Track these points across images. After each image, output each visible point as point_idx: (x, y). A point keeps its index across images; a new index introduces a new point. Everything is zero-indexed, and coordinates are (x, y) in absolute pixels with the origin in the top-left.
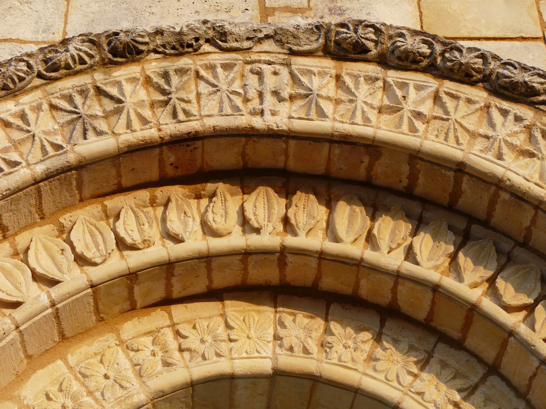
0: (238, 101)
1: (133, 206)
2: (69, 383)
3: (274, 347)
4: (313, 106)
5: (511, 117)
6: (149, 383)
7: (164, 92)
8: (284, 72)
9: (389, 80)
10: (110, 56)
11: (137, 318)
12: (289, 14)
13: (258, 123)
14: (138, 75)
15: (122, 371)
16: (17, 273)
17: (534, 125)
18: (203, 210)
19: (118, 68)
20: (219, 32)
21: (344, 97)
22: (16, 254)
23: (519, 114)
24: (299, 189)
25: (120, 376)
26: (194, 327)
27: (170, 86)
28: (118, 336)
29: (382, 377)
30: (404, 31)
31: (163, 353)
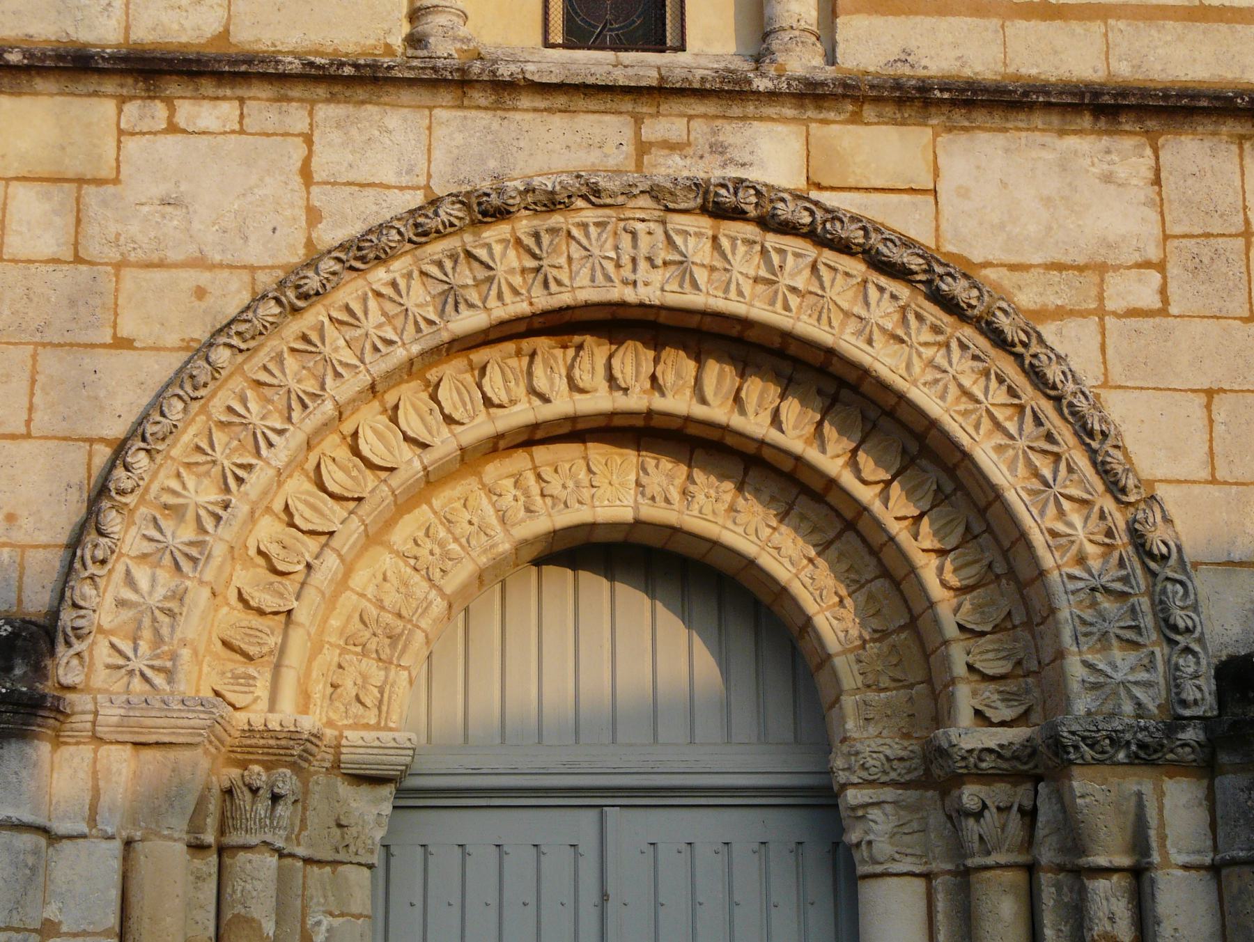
0: (610, 267)
1: (499, 360)
3: (636, 496)
4: (687, 276)
5: (887, 296)
7: (535, 257)
8: (658, 229)
9: (768, 245)
10: (480, 217)
12: (666, 152)
13: (630, 295)
14: (508, 236)
16: (389, 435)
17: (909, 306)
18: (569, 361)
19: (487, 227)
20: (592, 189)
21: (719, 263)
23: (895, 292)
24: (667, 345)
26: (556, 471)
27: (541, 250)
28: (481, 479)
29: (740, 530)
30: (786, 196)
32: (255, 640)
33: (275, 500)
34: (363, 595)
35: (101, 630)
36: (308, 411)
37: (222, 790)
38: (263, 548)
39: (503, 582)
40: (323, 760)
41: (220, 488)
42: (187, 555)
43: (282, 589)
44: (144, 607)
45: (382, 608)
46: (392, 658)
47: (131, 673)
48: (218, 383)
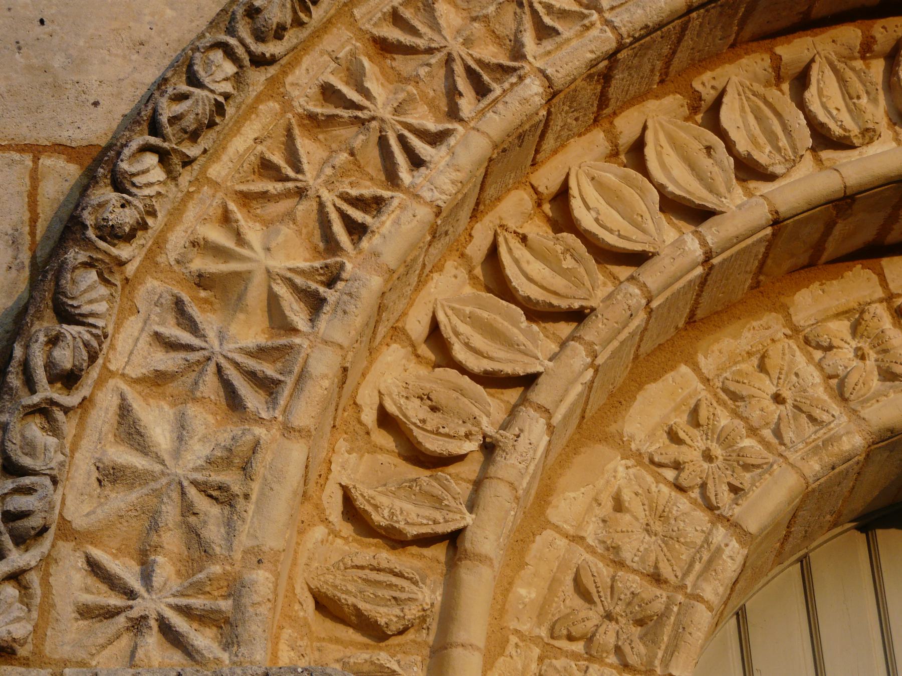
1: (834, 58)
2: (711, 410)
6: (865, 413)
11: (818, 283)
15: (808, 389)
16: (629, 193)
22: (613, 155)
25: (806, 398)
28: (788, 317)
31: (878, 353)
32: (387, 593)
33: (411, 312)
34: (579, 539)
35: (66, 531)
36: (491, 97)
38: (391, 408)
39: (804, 563)
41: (315, 248)
42: (252, 376)
43: (437, 490)
44: (164, 481)
45: (620, 564)
46: (651, 662)
47: (138, 625)
48: (304, 33)
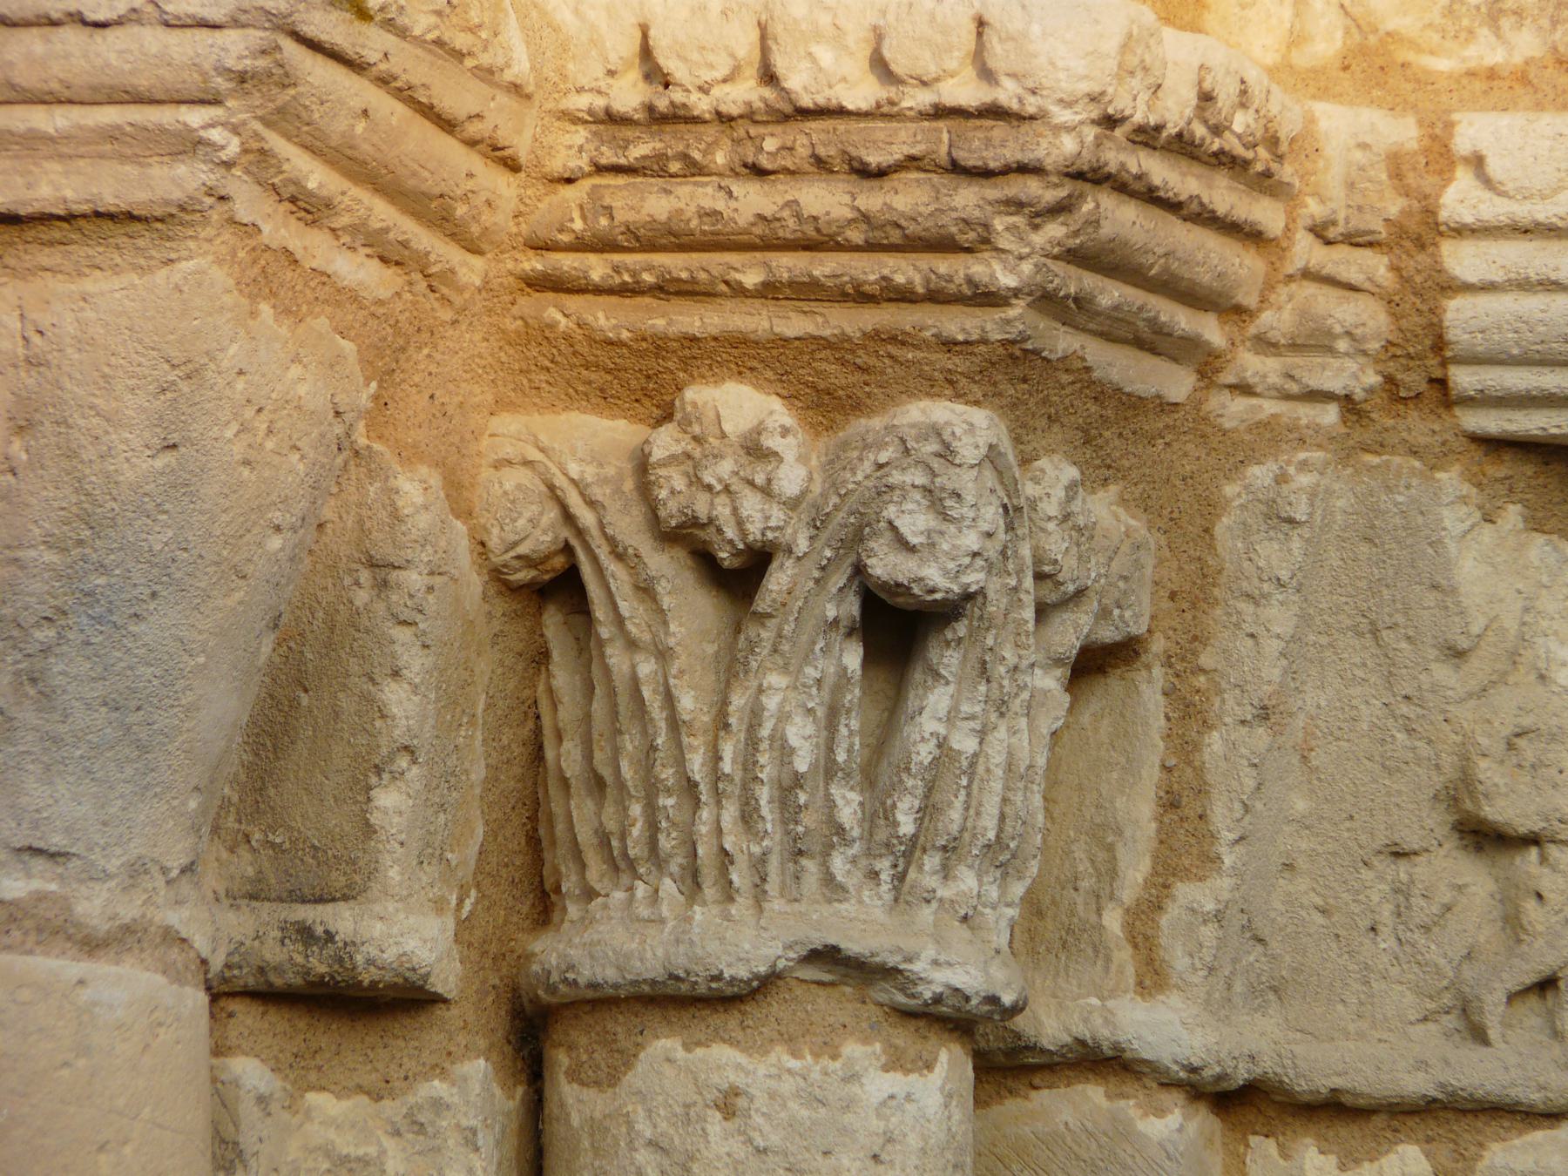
37: (497, 575)
40: (1314, 341)
